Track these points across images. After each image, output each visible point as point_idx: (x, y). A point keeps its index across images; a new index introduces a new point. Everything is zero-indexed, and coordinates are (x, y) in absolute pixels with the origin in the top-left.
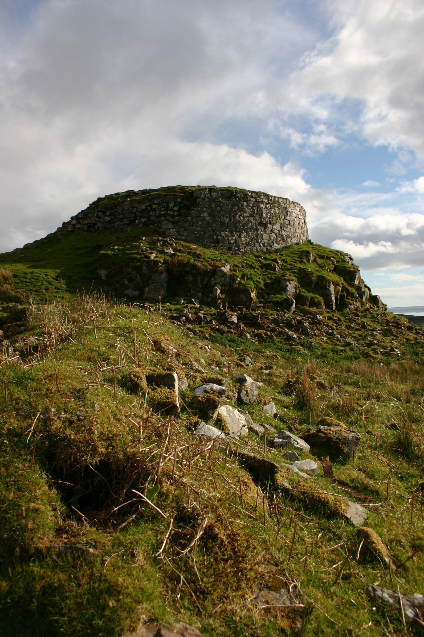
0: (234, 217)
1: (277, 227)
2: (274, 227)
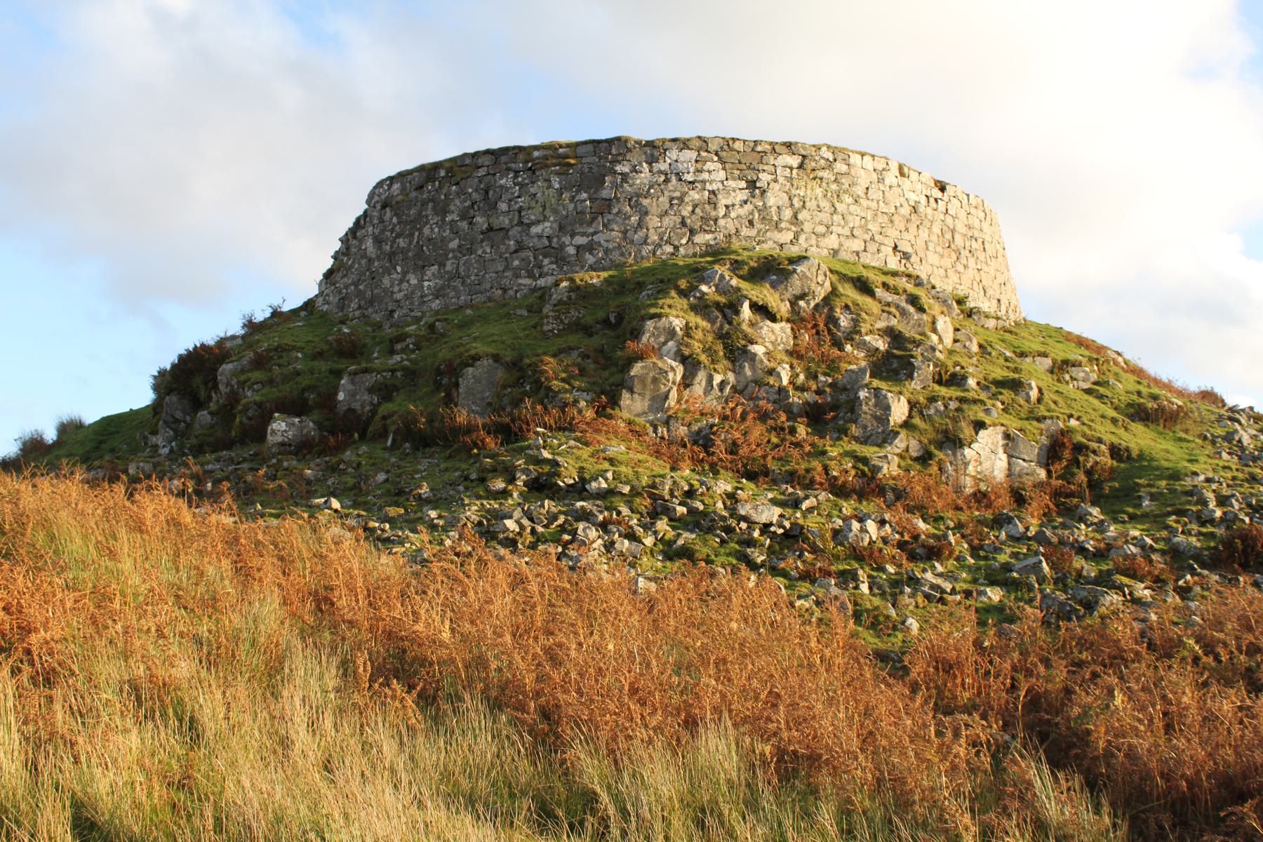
0: (420, 230)
1: (546, 228)
2: (535, 230)
